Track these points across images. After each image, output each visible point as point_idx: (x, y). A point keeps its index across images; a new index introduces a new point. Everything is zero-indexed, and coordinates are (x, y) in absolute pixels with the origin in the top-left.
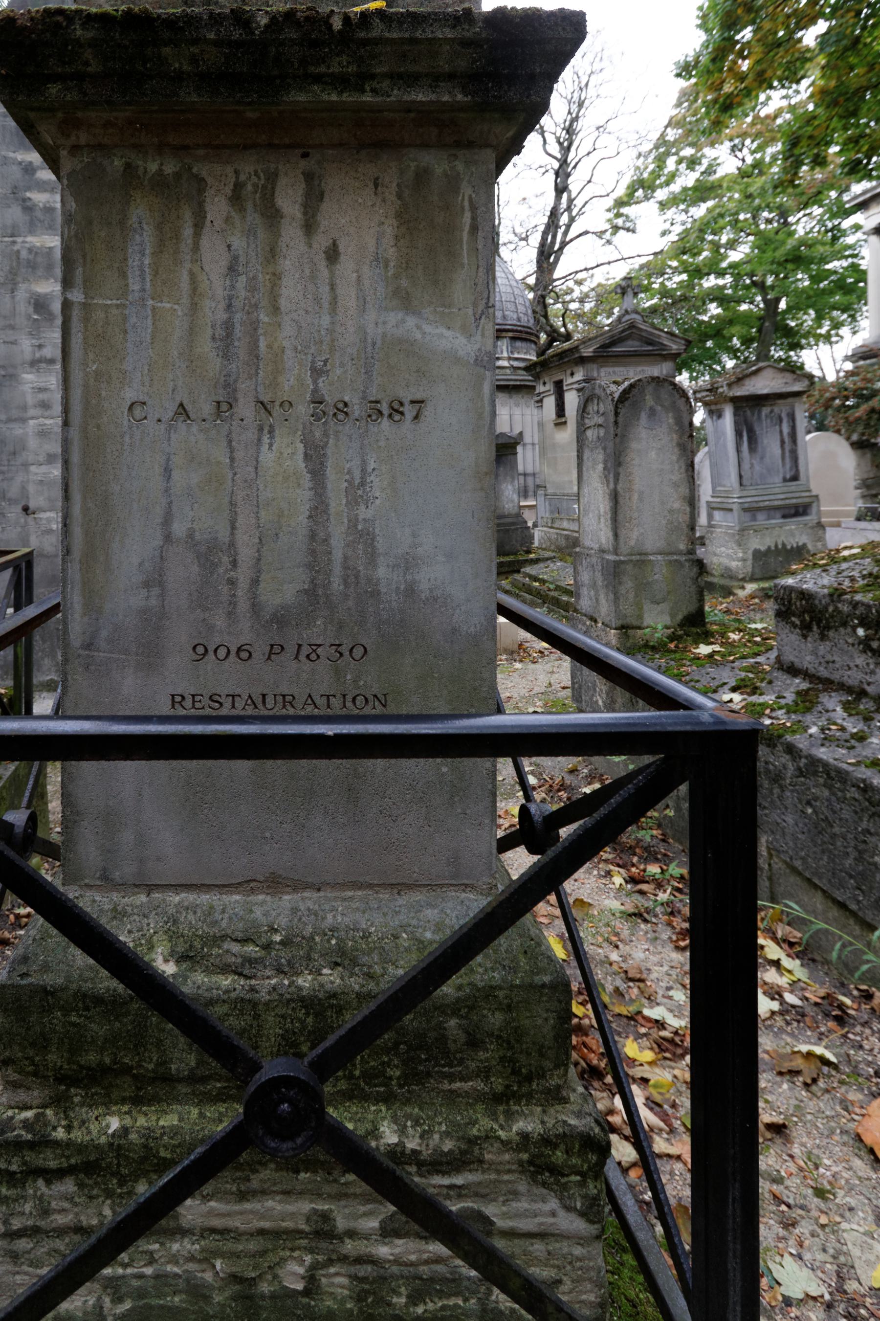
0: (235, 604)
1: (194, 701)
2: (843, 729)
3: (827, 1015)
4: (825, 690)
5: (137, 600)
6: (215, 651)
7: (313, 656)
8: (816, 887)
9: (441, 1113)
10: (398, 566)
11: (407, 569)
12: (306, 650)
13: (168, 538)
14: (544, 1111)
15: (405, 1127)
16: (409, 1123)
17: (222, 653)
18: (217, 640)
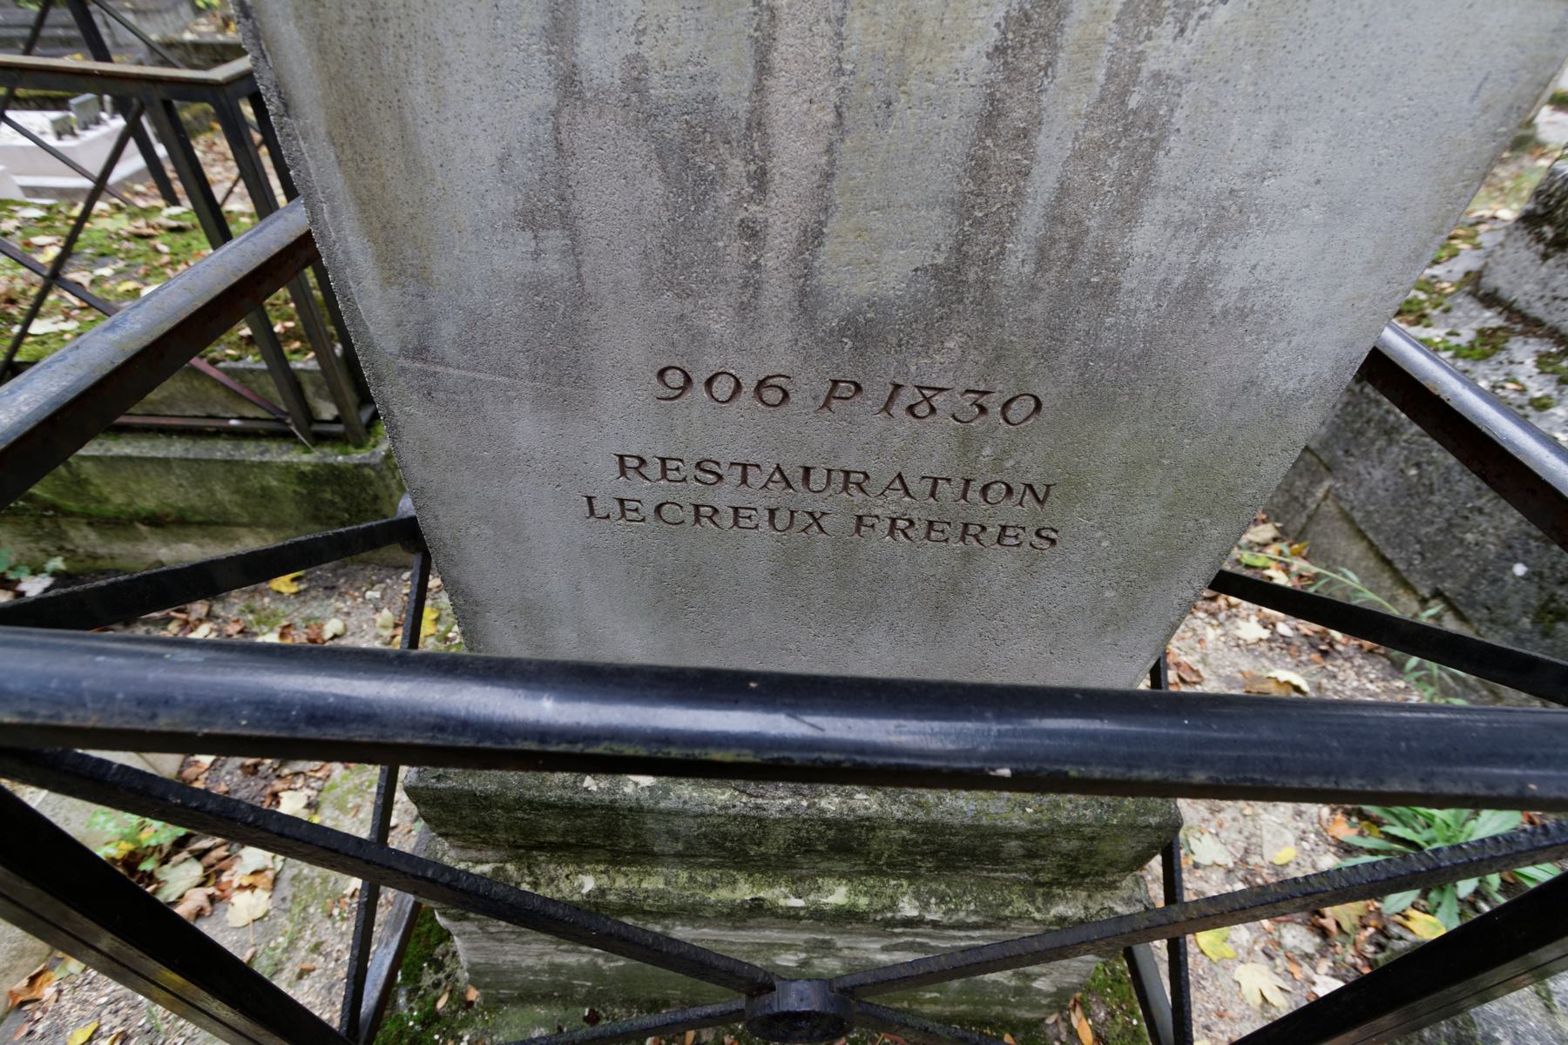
0: (758, 287)
1: (664, 470)
2: (1523, 390)
3: (1313, 646)
4: (1521, 333)
5: (511, 256)
6: (709, 383)
7: (923, 410)
8: (1364, 537)
9: (971, 892)
10: (1193, 225)
11: (1212, 233)
12: (908, 396)
13: (569, 83)
14: (1090, 896)
15: (928, 904)
16: (933, 900)
17: (723, 387)
18: (712, 363)
